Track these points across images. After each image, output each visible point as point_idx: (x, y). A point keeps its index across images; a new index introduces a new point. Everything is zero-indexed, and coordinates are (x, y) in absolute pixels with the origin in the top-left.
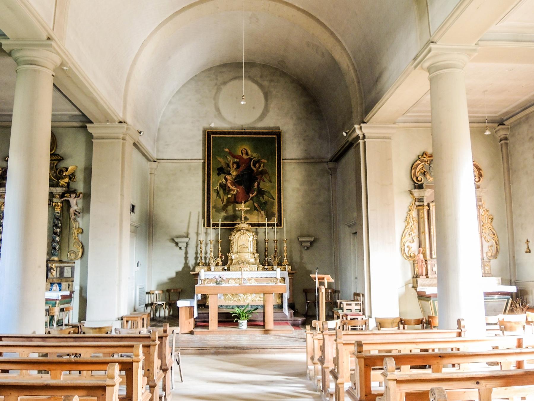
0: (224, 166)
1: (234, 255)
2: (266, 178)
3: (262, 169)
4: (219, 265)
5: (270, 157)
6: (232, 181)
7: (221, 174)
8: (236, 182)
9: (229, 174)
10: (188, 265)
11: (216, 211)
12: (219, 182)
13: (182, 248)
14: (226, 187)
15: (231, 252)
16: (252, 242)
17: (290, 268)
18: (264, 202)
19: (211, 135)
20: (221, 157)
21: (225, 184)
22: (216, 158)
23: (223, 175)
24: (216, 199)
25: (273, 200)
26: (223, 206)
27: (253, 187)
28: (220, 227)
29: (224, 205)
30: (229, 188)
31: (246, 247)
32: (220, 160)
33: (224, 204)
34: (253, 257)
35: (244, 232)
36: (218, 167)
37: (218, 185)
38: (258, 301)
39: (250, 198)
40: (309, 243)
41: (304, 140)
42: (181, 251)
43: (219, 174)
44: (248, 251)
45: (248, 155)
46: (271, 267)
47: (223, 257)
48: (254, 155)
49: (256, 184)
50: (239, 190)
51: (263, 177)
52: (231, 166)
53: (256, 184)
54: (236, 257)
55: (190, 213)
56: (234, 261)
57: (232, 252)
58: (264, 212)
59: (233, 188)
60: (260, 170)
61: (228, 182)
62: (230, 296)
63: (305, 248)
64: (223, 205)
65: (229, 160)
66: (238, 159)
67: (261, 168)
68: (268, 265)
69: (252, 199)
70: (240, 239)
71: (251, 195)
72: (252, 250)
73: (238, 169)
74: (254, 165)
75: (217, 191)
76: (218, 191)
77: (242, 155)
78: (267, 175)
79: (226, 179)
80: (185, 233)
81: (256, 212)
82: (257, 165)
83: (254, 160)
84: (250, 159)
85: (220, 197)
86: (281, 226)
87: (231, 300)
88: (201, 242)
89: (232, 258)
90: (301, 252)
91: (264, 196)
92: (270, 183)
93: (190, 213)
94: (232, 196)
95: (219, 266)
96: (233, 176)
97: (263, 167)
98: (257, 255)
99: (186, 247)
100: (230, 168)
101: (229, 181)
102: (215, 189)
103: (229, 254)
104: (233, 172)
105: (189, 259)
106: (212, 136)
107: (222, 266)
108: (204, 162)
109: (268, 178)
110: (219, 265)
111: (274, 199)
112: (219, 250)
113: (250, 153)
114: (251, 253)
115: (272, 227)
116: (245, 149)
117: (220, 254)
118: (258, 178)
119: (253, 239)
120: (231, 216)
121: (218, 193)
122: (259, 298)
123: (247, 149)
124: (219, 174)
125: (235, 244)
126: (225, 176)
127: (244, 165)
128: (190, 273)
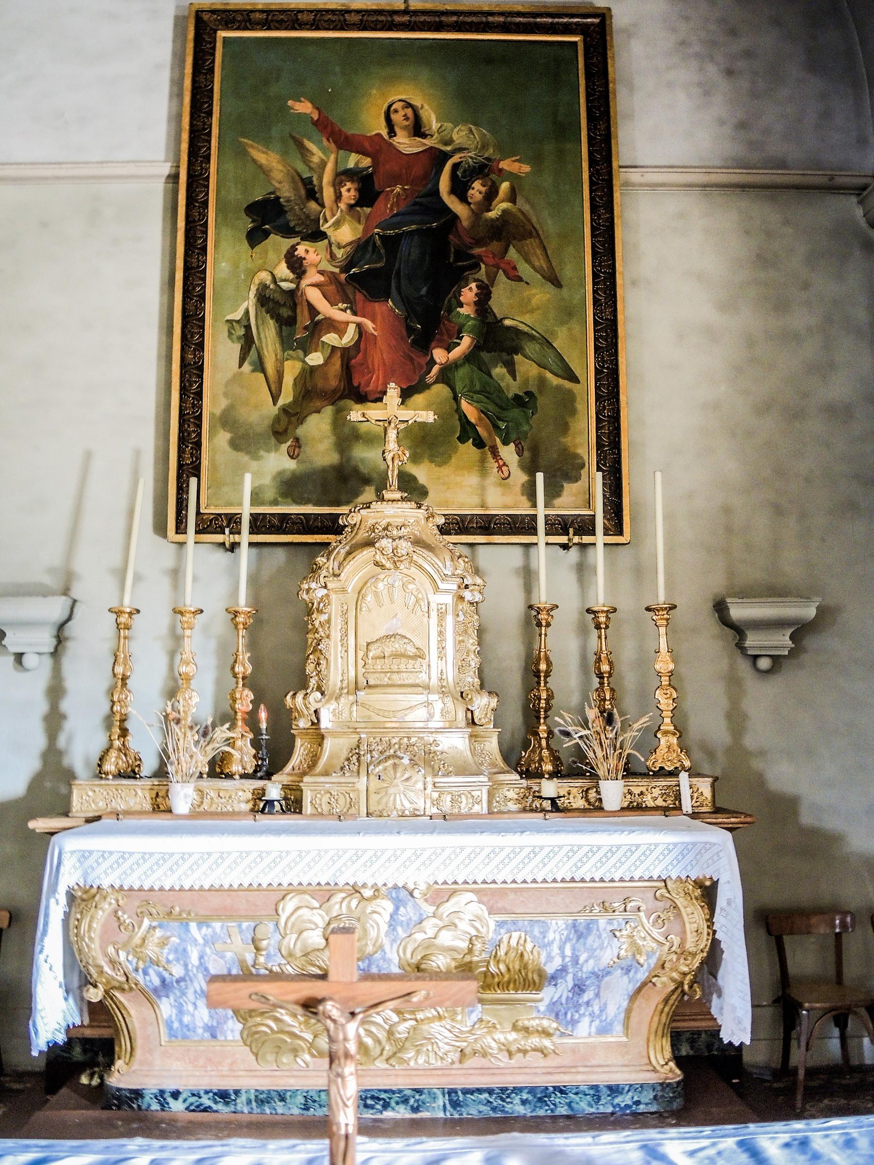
0: (286, 192)
1: (333, 705)
2: (528, 261)
3: (504, 211)
4: (236, 768)
5: (549, 147)
6: (333, 277)
7: (266, 234)
8: (352, 278)
9: (317, 235)
10: (66, 762)
11: (235, 444)
12: (257, 281)
13: (30, 660)
14: (294, 307)
15: (313, 682)
16: (450, 619)
17: (707, 793)
18: (517, 397)
19: (215, 31)
20: (266, 142)
21: (292, 293)
22: (242, 153)
23: (278, 244)
24: (236, 378)
25: (567, 384)
26: (277, 420)
27: (450, 310)
28: (245, 538)
29: (284, 410)
30: (313, 311)
31: (411, 651)
32: (261, 158)
33: (281, 402)
34: (461, 715)
35: (402, 551)
36: (251, 200)
37: (252, 294)
38: (504, 1057)
39: (435, 369)
40: (789, 632)
41: (730, 73)
42: (21, 676)
43: (255, 237)
44: (423, 677)
45: (424, 136)
46: (579, 783)
47: (263, 715)
48: (460, 135)
49: (469, 294)
50: (369, 324)
51: (512, 254)
52: (328, 193)
53: (469, 294)
54: (345, 715)
55: (88, 456)
56: (328, 744)
57: (319, 689)
58: (520, 453)
59: (337, 313)
60: (492, 214)
61: (304, 283)
62: (287, 1019)
63: (764, 664)
64: (274, 410)
65: (315, 159)
66: (365, 154)
67: (500, 207)
68: (555, 774)
69: (446, 375)
70: (369, 598)
71: (440, 355)
72: (451, 675)
73: (368, 210)
74: (460, 189)
75: (241, 332)
76: (248, 328)
77: (392, 132)
78: (531, 244)
79: (297, 266)
80: (51, 571)
81: (468, 449)
82: (477, 190)
83: (456, 159)
84: (438, 158)
85: (260, 366)
86: (620, 533)
87: (295, 1052)
88: (123, 619)
89: (316, 724)
90: (733, 683)
91: (518, 358)
92: (550, 287)
93: (88, 456)
94: (327, 361)
95: (230, 776)
96: (339, 247)
97: (512, 198)
98: (483, 703)
99: (56, 654)
100: (322, 205)
101: (312, 277)
102: (229, 317)
103: (300, 697)
104: (337, 224)
105: (68, 726)
106: (222, 34)
107: (252, 776)
108: (174, 178)
109: (540, 262)
110: (236, 768)
111: (574, 379)
112: (239, 669)
113: (432, 120)
114: (443, 691)
115: (563, 539)
116: (409, 105)
117: (245, 700)
118: (480, 258)
119: (462, 598)
120: (324, 470)
121: (248, 342)
122: (512, 1036)
123: (417, 102)
124: (255, 237)
125: (336, 634)
126: (294, 248)
127: (398, 189)
128: (32, 825)
